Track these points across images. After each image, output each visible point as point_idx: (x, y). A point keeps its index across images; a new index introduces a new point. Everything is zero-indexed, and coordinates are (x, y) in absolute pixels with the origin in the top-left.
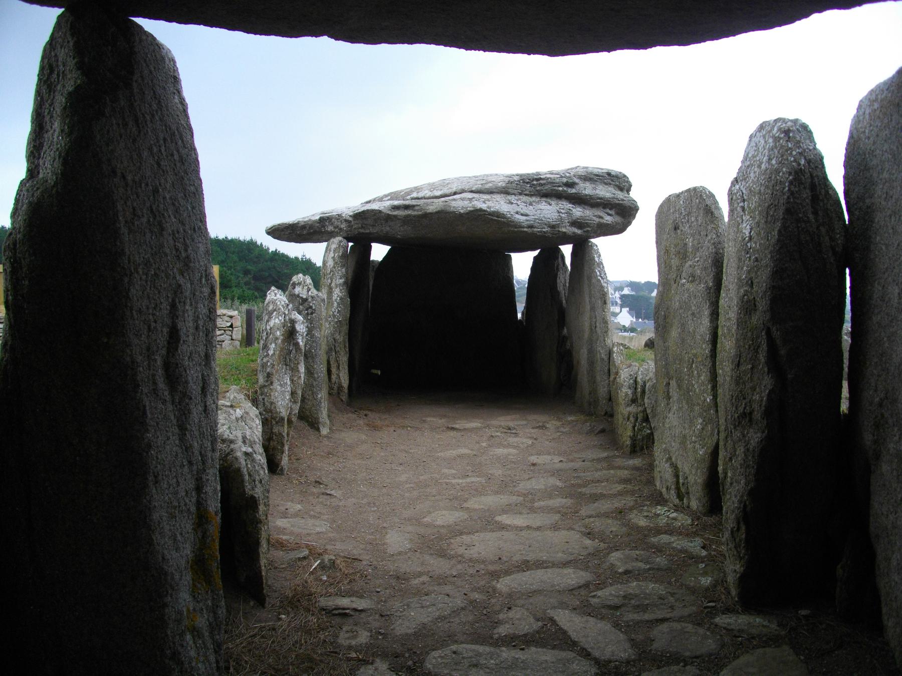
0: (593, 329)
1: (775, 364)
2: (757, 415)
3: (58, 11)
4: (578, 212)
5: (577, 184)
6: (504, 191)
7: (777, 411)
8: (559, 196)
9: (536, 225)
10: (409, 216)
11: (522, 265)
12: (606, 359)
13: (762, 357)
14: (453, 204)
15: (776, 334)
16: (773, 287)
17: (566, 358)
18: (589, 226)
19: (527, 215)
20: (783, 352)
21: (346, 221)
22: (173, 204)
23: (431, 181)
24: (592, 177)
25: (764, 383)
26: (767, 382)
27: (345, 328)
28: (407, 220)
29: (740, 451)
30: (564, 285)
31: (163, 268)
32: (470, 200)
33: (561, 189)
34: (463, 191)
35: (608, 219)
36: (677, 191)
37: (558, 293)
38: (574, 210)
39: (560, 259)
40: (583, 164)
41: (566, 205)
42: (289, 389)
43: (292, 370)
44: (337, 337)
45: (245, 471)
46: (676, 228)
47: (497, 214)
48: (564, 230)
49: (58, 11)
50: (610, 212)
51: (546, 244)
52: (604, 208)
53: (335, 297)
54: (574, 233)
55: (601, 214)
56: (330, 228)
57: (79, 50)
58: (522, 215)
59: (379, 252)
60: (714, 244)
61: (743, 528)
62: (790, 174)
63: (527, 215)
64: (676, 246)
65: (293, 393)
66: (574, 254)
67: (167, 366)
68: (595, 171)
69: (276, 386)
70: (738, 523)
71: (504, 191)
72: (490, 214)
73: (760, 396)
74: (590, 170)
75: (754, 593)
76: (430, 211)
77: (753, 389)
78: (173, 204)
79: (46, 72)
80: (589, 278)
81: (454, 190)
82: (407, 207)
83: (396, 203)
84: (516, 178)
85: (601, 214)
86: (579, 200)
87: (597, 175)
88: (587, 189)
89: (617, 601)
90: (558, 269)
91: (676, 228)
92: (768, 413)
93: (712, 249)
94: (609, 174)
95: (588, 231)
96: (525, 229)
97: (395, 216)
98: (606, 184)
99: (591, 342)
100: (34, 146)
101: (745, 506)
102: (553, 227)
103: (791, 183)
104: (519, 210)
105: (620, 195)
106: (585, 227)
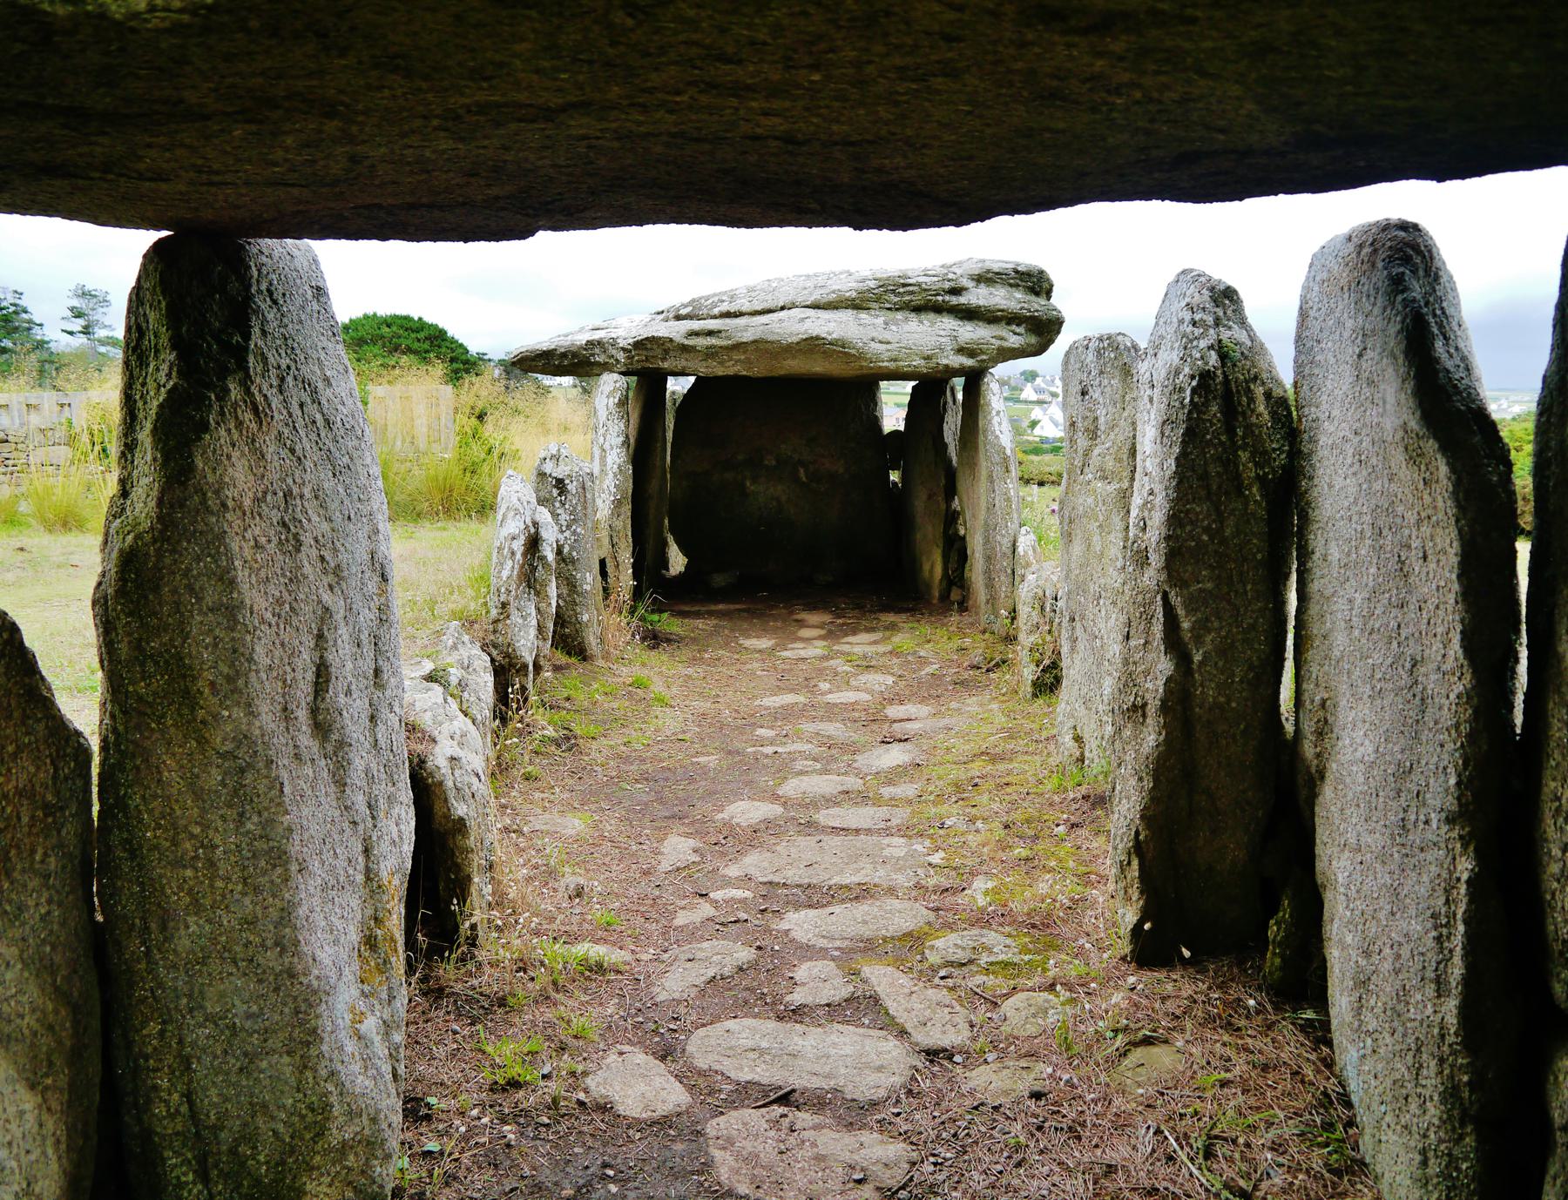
1: (1174, 642)
2: (1153, 705)
3: (147, 238)
4: (970, 332)
6: (857, 304)
7: (1179, 703)
8: (938, 309)
12: (1009, 553)
13: (1158, 629)
14: (776, 328)
15: (1176, 600)
16: (1168, 538)
17: (956, 550)
18: (983, 353)
20: (1186, 625)
22: (316, 497)
24: (986, 278)
25: (1160, 667)
26: (1164, 666)
27: (627, 509)
28: (711, 353)
29: (1129, 757)
31: (302, 596)
32: (802, 320)
37: (945, 446)
41: (948, 323)
42: (534, 622)
43: (538, 594)
44: (619, 524)
45: (450, 784)
46: (1084, 393)
48: (945, 362)
49: (147, 238)
52: (1008, 324)
53: (609, 460)
55: (1004, 333)
56: (601, 359)
57: (174, 317)
59: (678, 386)
61: (1135, 863)
62: (1193, 377)
65: (540, 628)
67: (314, 711)
68: (996, 267)
69: (515, 618)
70: (1129, 854)
71: (857, 304)
73: (1154, 689)
74: (988, 265)
75: (1150, 950)
77: (1146, 673)
78: (316, 497)
79: (135, 335)
81: (781, 304)
83: (696, 325)
84: (872, 284)
86: (969, 314)
88: (978, 296)
89: (962, 956)
90: (945, 410)
91: (1084, 393)
92: (1164, 708)
94: (1017, 272)
98: (1011, 285)
99: (990, 530)
100: (126, 445)
101: (1137, 833)
102: (928, 358)
103: (1194, 391)
104: (875, 334)
105: (1036, 304)
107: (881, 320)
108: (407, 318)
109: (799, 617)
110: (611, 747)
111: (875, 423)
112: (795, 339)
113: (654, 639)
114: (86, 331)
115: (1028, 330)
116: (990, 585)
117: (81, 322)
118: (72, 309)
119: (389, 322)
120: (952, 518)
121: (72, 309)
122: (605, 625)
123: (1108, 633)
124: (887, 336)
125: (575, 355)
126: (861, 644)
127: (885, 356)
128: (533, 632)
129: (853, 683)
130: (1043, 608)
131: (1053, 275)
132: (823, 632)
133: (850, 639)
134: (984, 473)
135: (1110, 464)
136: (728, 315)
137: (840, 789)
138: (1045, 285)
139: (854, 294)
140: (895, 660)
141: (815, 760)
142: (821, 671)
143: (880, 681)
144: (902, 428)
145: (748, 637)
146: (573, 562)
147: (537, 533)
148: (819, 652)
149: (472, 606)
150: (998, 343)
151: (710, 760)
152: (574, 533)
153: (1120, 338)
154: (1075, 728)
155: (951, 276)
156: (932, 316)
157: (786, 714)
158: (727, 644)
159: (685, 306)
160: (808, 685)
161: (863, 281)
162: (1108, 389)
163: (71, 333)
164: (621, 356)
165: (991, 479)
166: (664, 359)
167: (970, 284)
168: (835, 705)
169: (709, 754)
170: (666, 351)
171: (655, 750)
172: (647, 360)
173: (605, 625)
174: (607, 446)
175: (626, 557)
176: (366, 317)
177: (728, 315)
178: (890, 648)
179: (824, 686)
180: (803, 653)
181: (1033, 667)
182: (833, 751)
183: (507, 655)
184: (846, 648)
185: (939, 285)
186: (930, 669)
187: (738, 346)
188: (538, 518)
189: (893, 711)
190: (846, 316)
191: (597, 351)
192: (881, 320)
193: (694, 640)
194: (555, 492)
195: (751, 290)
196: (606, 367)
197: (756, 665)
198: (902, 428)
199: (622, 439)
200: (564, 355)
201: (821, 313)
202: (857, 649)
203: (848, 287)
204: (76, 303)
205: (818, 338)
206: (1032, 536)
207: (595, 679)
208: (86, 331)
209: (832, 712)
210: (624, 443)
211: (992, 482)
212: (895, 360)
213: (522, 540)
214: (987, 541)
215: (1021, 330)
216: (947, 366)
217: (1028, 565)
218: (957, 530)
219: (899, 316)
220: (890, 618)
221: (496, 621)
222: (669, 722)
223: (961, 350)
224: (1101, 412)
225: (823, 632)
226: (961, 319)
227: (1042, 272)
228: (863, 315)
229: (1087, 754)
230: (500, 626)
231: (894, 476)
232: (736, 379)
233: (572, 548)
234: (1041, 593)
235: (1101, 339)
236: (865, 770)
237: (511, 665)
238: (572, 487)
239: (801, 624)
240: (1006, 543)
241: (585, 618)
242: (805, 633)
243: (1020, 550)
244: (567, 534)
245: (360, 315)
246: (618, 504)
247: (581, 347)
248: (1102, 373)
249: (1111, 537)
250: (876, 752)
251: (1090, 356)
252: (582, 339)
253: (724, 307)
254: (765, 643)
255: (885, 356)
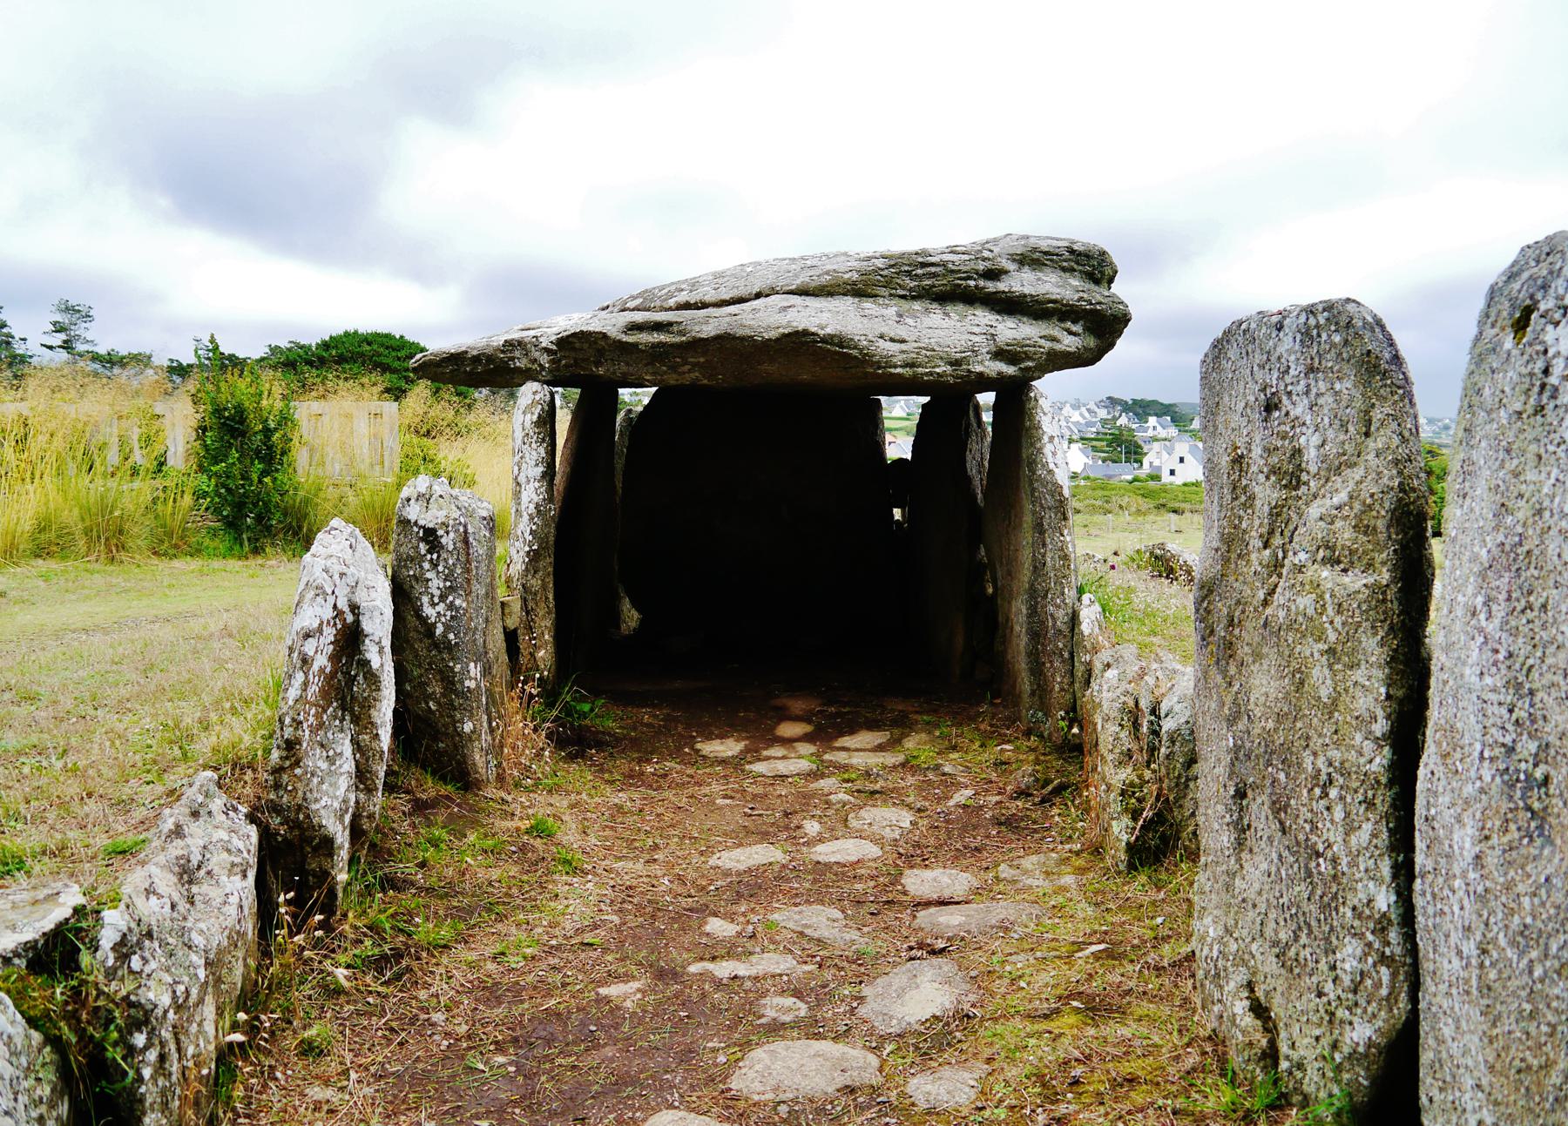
0: (1038, 568)
4: (1012, 330)
5: (1006, 272)
6: (860, 289)
9: (921, 359)
10: (661, 344)
11: (899, 425)
17: (988, 621)
18: (1029, 358)
19: (903, 341)
21: (546, 350)
23: (720, 268)
24: (1033, 259)
27: (547, 562)
30: (981, 465)
32: (785, 309)
33: (972, 283)
34: (772, 292)
35: (1069, 343)
36: (1274, 304)
37: (969, 480)
38: (1000, 327)
39: (971, 414)
40: (1019, 230)
41: (983, 317)
43: (356, 720)
44: (535, 583)
46: (1270, 407)
47: (839, 341)
48: (979, 368)
50: (1074, 328)
51: (947, 401)
52: (1061, 320)
53: (525, 497)
54: (999, 373)
55: (1056, 332)
58: (892, 340)
59: (636, 398)
60: (1396, 462)
63: (903, 341)
64: (1269, 451)
66: (997, 408)
69: (315, 760)
71: (860, 289)
72: (824, 340)
74: (1033, 242)
76: (704, 336)
80: (1032, 464)
81: (756, 289)
82: (658, 327)
83: (639, 317)
84: (880, 263)
85: (1056, 332)
86: (1011, 306)
87: (1046, 253)
88: (1023, 282)
90: (968, 435)
91: (1270, 407)
93: (1390, 478)
94: (1072, 251)
95: (1028, 369)
96: (899, 370)
97: (635, 345)
98: (1064, 270)
99: (1036, 597)
102: (956, 363)
104: (884, 330)
105: (1097, 294)
106: (1023, 360)
107: (892, 311)
108: (388, 336)
109: (778, 702)
110: (471, 966)
111: (879, 449)
112: (773, 334)
113: (574, 742)
114: (67, 346)
115: (1086, 329)
116: (1037, 670)
117: (63, 336)
118: (55, 324)
119: (369, 339)
120: (977, 573)
121: (55, 324)
122: (503, 731)
123: (1353, 864)
124: (901, 332)
125: (490, 358)
126: (860, 750)
127: (898, 360)
128: (344, 783)
129: (853, 823)
130: (1136, 725)
131: (1116, 257)
132: (808, 728)
133: (846, 741)
134: (1028, 519)
135: (1345, 534)
136: (687, 306)
137: (841, 1080)
138: (1108, 271)
139: (855, 276)
140: (910, 780)
141: (797, 994)
142: (806, 797)
143: (892, 819)
144: (909, 456)
145: (709, 737)
146: (450, 647)
147: (357, 622)
148: (804, 765)
149: (247, 739)
150: (1048, 345)
151: (626, 992)
152: (451, 607)
153: (1350, 307)
154: (1250, 986)
155: (986, 254)
156: (960, 307)
157: (753, 888)
158: (679, 749)
159: (634, 298)
160: (785, 828)
161: (869, 259)
162: (1327, 400)
163: (51, 348)
164: (544, 360)
165: (1039, 528)
166: (598, 364)
167: (1011, 267)
168: (828, 866)
169: (627, 978)
170: (601, 352)
171: (540, 970)
172: (576, 364)
173: (503, 731)
174: (522, 479)
175: (545, 625)
176: (347, 334)
177: (687, 306)
178: (901, 758)
179: (812, 827)
180: (782, 767)
181: (1126, 820)
182: (828, 975)
183: (294, 825)
184: (841, 757)
185: (972, 265)
186: (962, 796)
187: (698, 344)
188: (361, 598)
189: (919, 882)
190: (846, 304)
191: (517, 354)
192: (892, 311)
193: (635, 744)
194: (423, 548)
195: (718, 276)
196: (528, 375)
197: (716, 787)
198: (909, 456)
199: (541, 469)
200: (476, 359)
201: (809, 301)
202: (858, 760)
203: (848, 270)
204: (59, 317)
205: (805, 333)
206: (1097, 608)
207: (475, 823)
208: (67, 346)
209: (827, 882)
210: (544, 475)
211: (1042, 532)
212: (912, 365)
213: (329, 634)
214: (1033, 611)
215: (1077, 328)
216: (981, 374)
217: (1095, 650)
218: (985, 589)
219: (917, 306)
220: (897, 706)
221: (278, 770)
222: (576, 903)
223: (1000, 354)
224: (1309, 442)
225: (808, 728)
226: (999, 312)
227: (1103, 253)
228: (868, 304)
229: (1284, 1048)
230: (285, 777)
231: (897, 514)
232: (694, 388)
233: (448, 628)
234: (1131, 703)
235: (1310, 310)
236: (882, 1029)
237: (309, 840)
238: (448, 541)
239: (786, 716)
240: (1061, 616)
241: (468, 727)
242: (788, 729)
243: (1085, 627)
244: (441, 608)
245: (341, 332)
246: (534, 558)
247: (497, 349)
248: (1311, 370)
249: (1359, 675)
250: (898, 977)
251: (1287, 344)
252: (499, 341)
253: (682, 298)
254: (729, 748)
255: (898, 360)
